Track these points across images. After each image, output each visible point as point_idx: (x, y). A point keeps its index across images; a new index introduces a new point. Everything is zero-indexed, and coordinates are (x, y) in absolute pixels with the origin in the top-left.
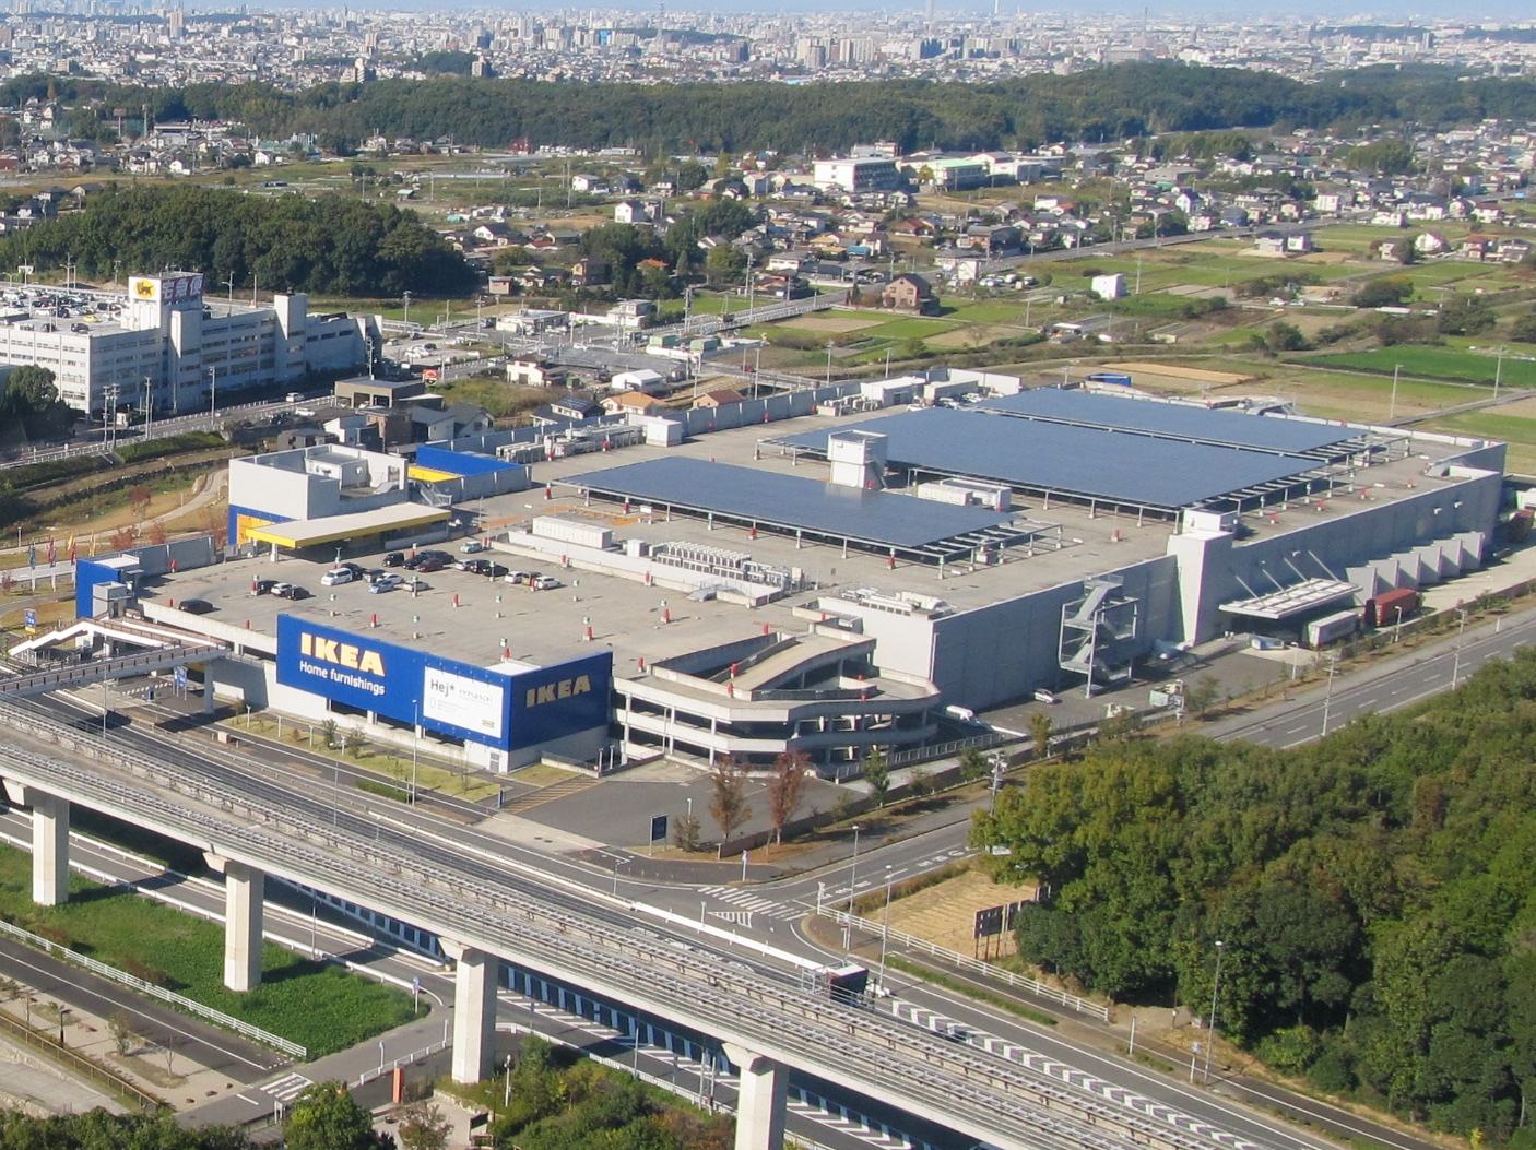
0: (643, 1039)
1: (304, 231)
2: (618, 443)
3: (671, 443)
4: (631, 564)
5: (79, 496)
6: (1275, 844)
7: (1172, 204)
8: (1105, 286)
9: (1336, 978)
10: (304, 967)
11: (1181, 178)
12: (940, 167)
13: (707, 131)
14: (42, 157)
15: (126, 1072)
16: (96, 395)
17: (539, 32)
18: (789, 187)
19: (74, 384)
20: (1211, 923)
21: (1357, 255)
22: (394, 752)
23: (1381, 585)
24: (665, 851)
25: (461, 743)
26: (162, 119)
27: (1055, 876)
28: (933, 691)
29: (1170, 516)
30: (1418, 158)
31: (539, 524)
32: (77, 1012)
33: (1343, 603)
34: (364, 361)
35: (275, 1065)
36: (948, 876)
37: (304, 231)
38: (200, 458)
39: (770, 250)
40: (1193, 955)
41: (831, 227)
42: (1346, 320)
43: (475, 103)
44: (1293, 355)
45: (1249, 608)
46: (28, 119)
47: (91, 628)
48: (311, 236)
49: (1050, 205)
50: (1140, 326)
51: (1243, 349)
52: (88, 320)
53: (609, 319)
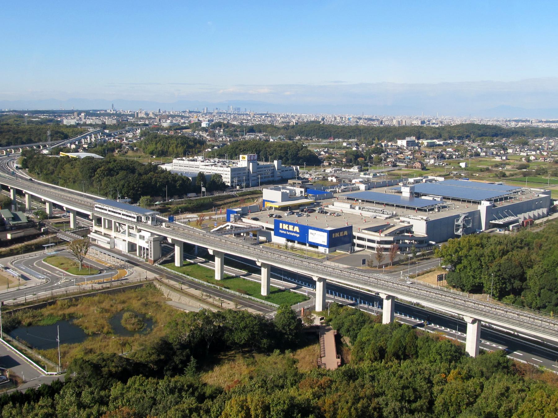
0: (361, 303)
1: (281, 150)
2: (353, 190)
4: (357, 211)
6: (504, 253)
7: (477, 150)
8: (463, 165)
9: (519, 282)
10: (280, 291)
11: (479, 145)
12: (425, 142)
13: (373, 136)
14: (221, 139)
16: (232, 182)
17: (335, 119)
18: (392, 145)
19: (227, 179)
20: (491, 270)
21: (517, 160)
22: (302, 250)
23: (525, 218)
24: (366, 267)
25: (318, 248)
26: (249, 132)
27: (455, 264)
28: (426, 236)
29: (479, 203)
30: (530, 143)
31: (335, 204)
32: (225, 300)
33: (516, 221)
34: (295, 176)
36: (430, 271)
37: (281, 150)
38: (256, 196)
39: (388, 157)
40: (486, 278)
41: (401, 153)
42: (515, 172)
43: (321, 129)
45: (497, 222)
46: (217, 132)
47: (230, 224)
49: (450, 150)
50: (470, 173)
51: (493, 177)
53: (351, 170)
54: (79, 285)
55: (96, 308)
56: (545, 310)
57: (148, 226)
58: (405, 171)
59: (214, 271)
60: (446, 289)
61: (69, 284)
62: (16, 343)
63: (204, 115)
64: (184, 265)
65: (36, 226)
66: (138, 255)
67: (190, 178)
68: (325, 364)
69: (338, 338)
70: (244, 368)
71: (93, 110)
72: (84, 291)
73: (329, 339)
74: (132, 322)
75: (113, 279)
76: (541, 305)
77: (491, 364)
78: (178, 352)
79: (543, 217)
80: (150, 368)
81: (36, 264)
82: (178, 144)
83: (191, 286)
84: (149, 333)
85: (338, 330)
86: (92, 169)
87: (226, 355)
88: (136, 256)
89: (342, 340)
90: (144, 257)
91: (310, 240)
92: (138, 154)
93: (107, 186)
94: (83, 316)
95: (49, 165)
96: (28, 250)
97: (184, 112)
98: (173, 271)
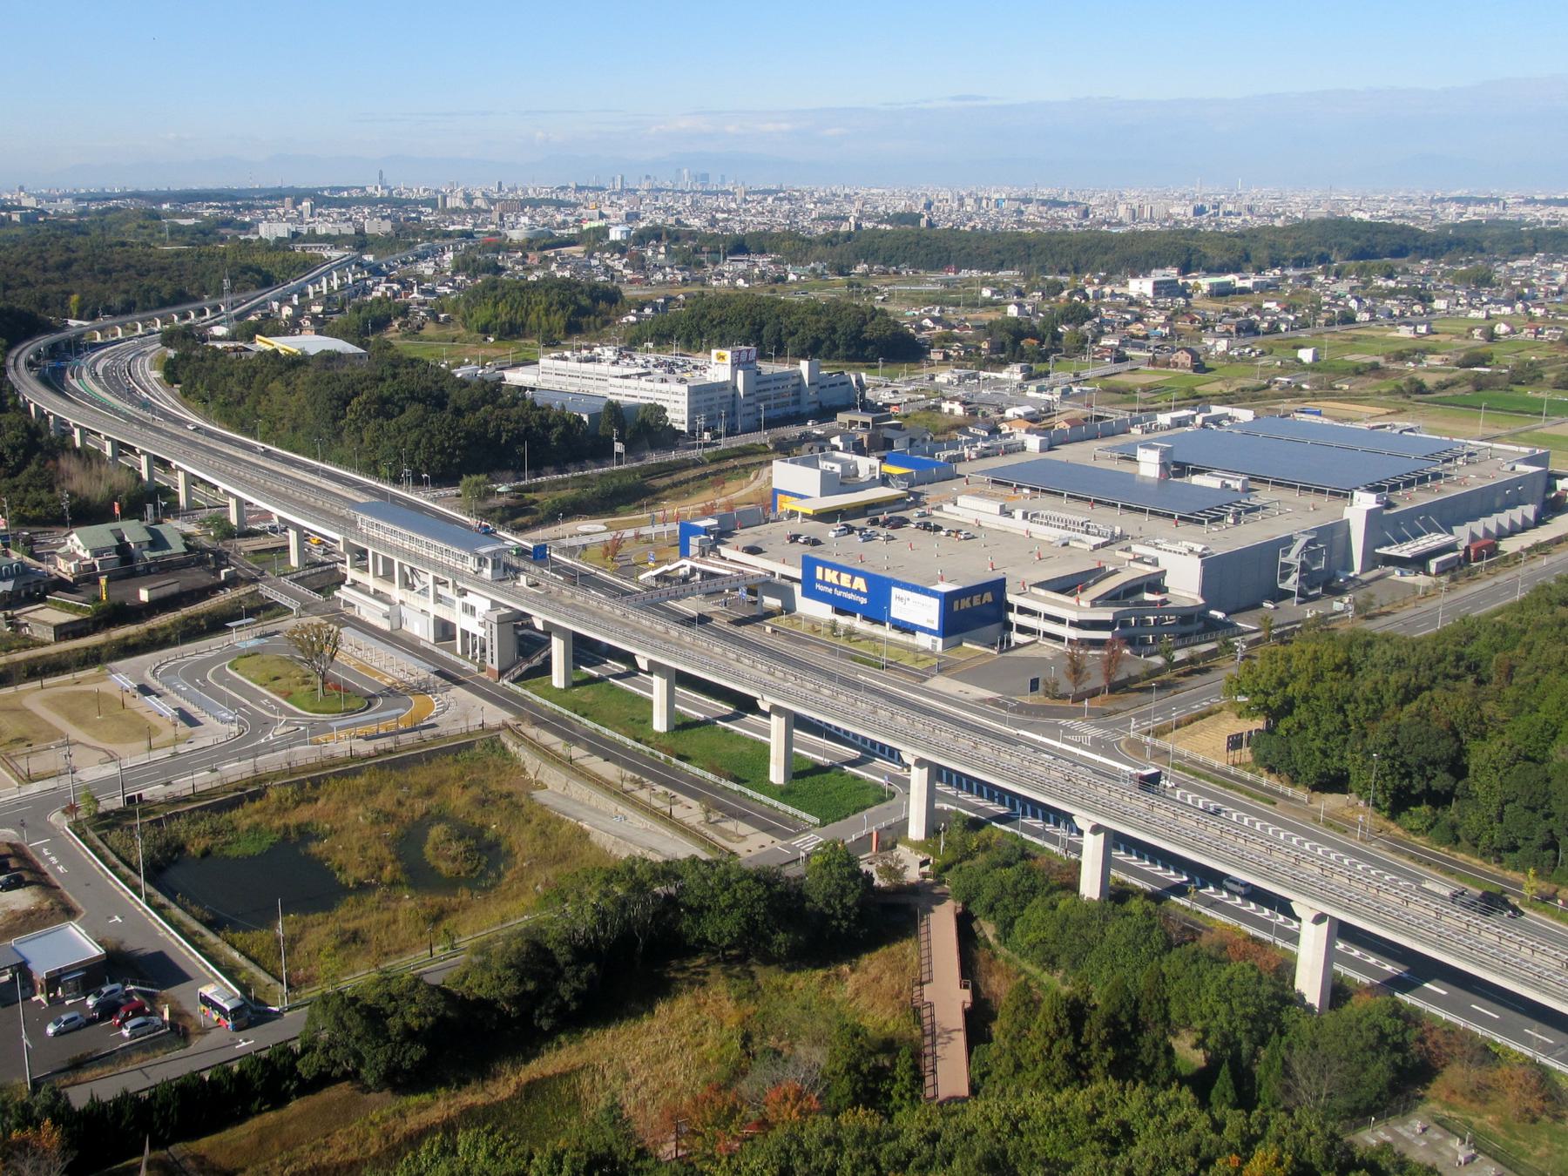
0: (1024, 813)
1: (818, 321)
2: (1009, 450)
3: (1041, 451)
4: (1017, 524)
5: (681, 483)
6: (1409, 694)
7: (1346, 305)
8: (1306, 355)
9: (1446, 776)
10: (818, 769)
11: (1352, 289)
12: (1205, 283)
14: (659, 276)
15: (710, 833)
16: (691, 421)
18: (1113, 295)
20: (1370, 742)
21: (1459, 336)
22: (873, 638)
25: (913, 633)
26: (732, 253)
27: (1276, 714)
28: (1201, 601)
29: (1345, 495)
30: (1496, 277)
32: (680, 797)
33: (1451, 548)
34: (855, 400)
35: (799, 829)
36: (1210, 714)
37: (818, 321)
39: (1102, 333)
41: (1139, 319)
42: (1453, 376)
43: (922, 243)
44: (1420, 397)
45: (1394, 551)
46: (650, 253)
48: (822, 325)
49: (1272, 305)
50: (1327, 379)
51: (1390, 393)
52: (687, 376)
53: (1004, 375)
54: (318, 743)
55: (361, 809)
56: (1514, 856)
57: (483, 581)
58: (1149, 376)
59: (650, 703)
60: (1249, 776)
61: (297, 738)
62: (177, 912)
63: (614, 198)
64: (576, 684)
65: (208, 561)
66: (459, 650)
67: (586, 418)
68: (931, 1005)
69: (965, 923)
70: (729, 1006)
71: (332, 189)
72: (333, 761)
73: (941, 924)
74: (451, 853)
75: (401, 727)
76: (1505, 843)
77: (1360, 1044)
78: (569, 972)
79: (1524, 529)
80: (500, 1012)
81: (213, 676)
82: (551, 305)
83: (594, 751)
84: (493, 886)
85: (966, 904)
86: (339, 399)
87: (684, 969)
88: (454, 656)
89: (975, 926)
90: (474, 658)
91: (895, 614)
92: (451, 331)
93: (376, 442)
94: (333, 831)
95: (231, 381)
96: (192, 631)
97: (562, 188)
98: (548, 703)
